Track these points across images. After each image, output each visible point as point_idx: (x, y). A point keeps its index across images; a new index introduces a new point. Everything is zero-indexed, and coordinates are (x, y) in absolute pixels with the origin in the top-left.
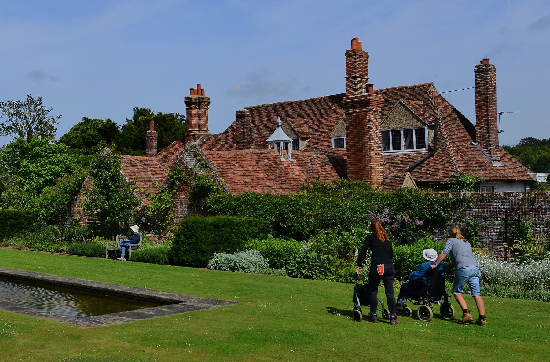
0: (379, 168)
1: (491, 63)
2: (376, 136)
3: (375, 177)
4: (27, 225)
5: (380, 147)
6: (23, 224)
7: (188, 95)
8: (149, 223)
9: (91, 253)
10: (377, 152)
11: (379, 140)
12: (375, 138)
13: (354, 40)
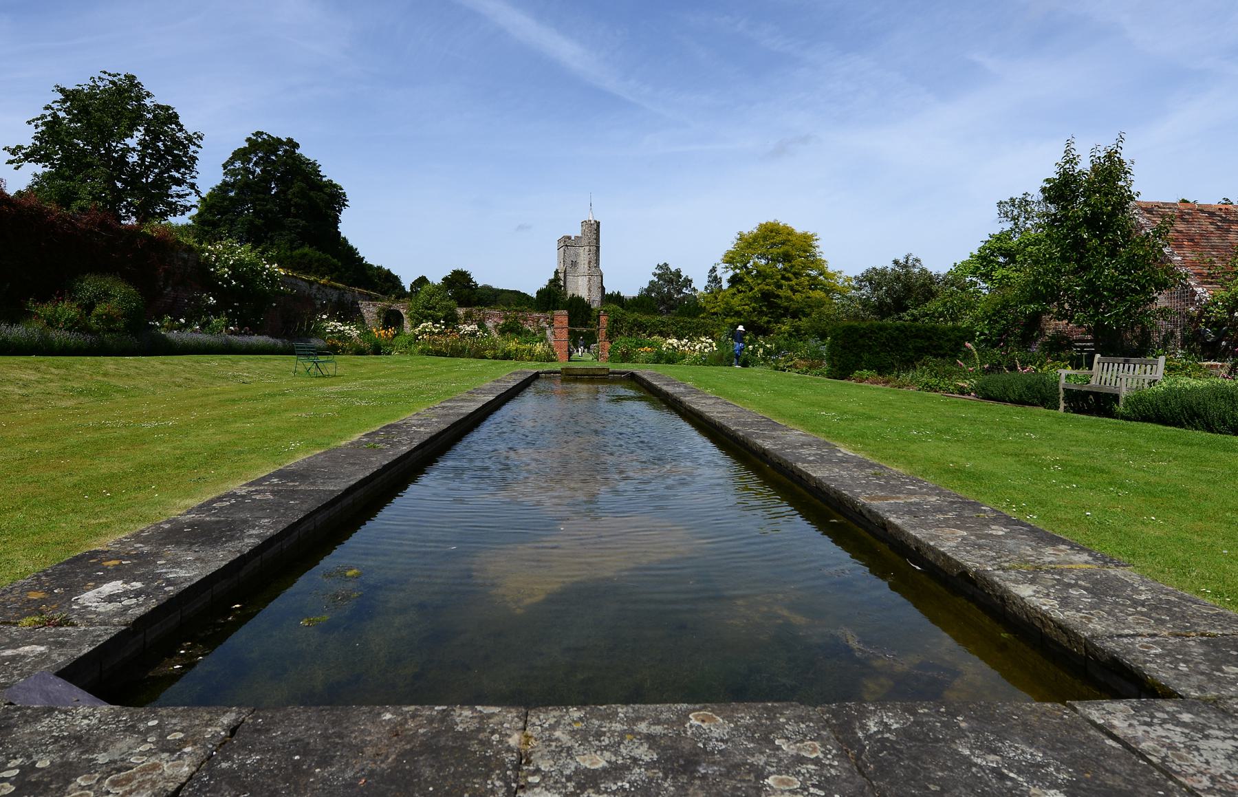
4: (951, 350)
6: (942, 349)
8: (1224, 343)
9: (1020, 396)
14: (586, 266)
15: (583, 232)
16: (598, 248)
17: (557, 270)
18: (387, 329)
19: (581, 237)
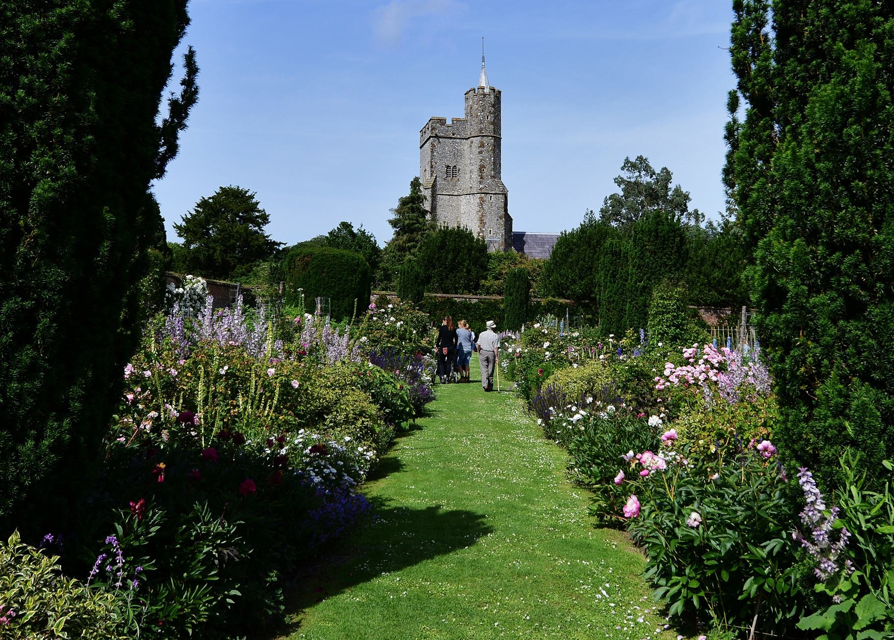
14: (475, 176)
15: (470, 112)
16: (497, 140)
17: (417, 179)
18: (806, 168)
19: (465, 121)
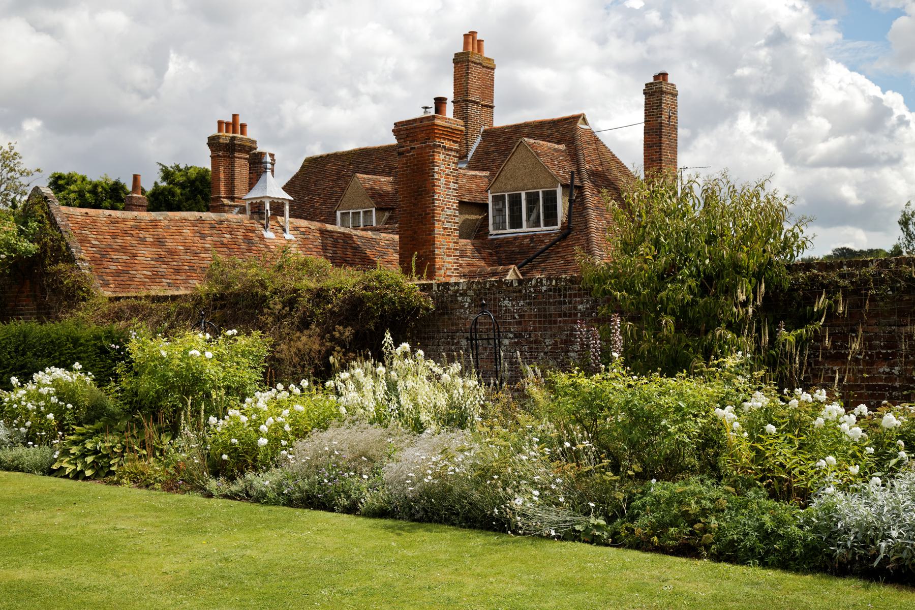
0: (451, 256)
1: (670, 80)
2: (447, 195)
3: (443, 271)
5: (454, 216)
7: (214, 131)
10: (448, 225)
11: (454, 203)
12: (445, 198)
13: (470, 37)
